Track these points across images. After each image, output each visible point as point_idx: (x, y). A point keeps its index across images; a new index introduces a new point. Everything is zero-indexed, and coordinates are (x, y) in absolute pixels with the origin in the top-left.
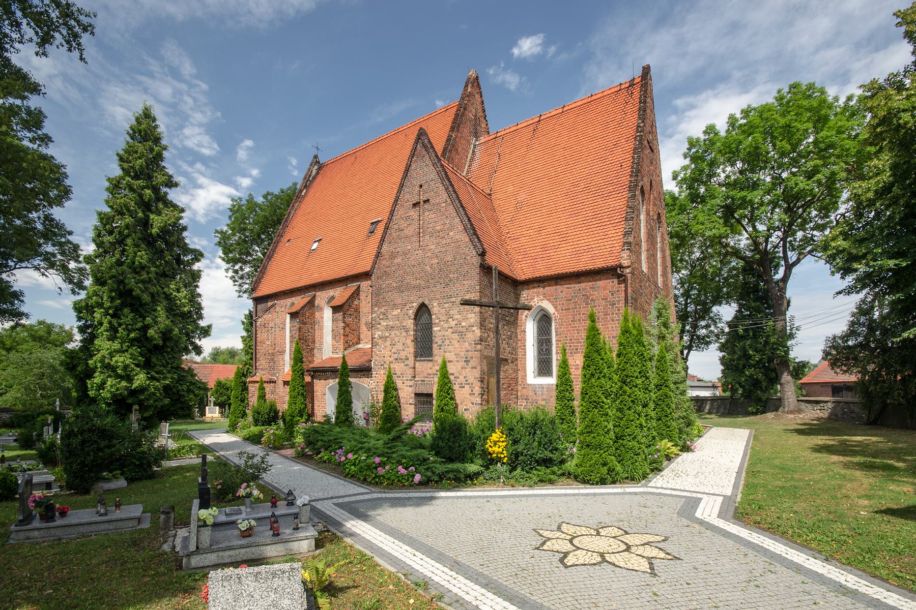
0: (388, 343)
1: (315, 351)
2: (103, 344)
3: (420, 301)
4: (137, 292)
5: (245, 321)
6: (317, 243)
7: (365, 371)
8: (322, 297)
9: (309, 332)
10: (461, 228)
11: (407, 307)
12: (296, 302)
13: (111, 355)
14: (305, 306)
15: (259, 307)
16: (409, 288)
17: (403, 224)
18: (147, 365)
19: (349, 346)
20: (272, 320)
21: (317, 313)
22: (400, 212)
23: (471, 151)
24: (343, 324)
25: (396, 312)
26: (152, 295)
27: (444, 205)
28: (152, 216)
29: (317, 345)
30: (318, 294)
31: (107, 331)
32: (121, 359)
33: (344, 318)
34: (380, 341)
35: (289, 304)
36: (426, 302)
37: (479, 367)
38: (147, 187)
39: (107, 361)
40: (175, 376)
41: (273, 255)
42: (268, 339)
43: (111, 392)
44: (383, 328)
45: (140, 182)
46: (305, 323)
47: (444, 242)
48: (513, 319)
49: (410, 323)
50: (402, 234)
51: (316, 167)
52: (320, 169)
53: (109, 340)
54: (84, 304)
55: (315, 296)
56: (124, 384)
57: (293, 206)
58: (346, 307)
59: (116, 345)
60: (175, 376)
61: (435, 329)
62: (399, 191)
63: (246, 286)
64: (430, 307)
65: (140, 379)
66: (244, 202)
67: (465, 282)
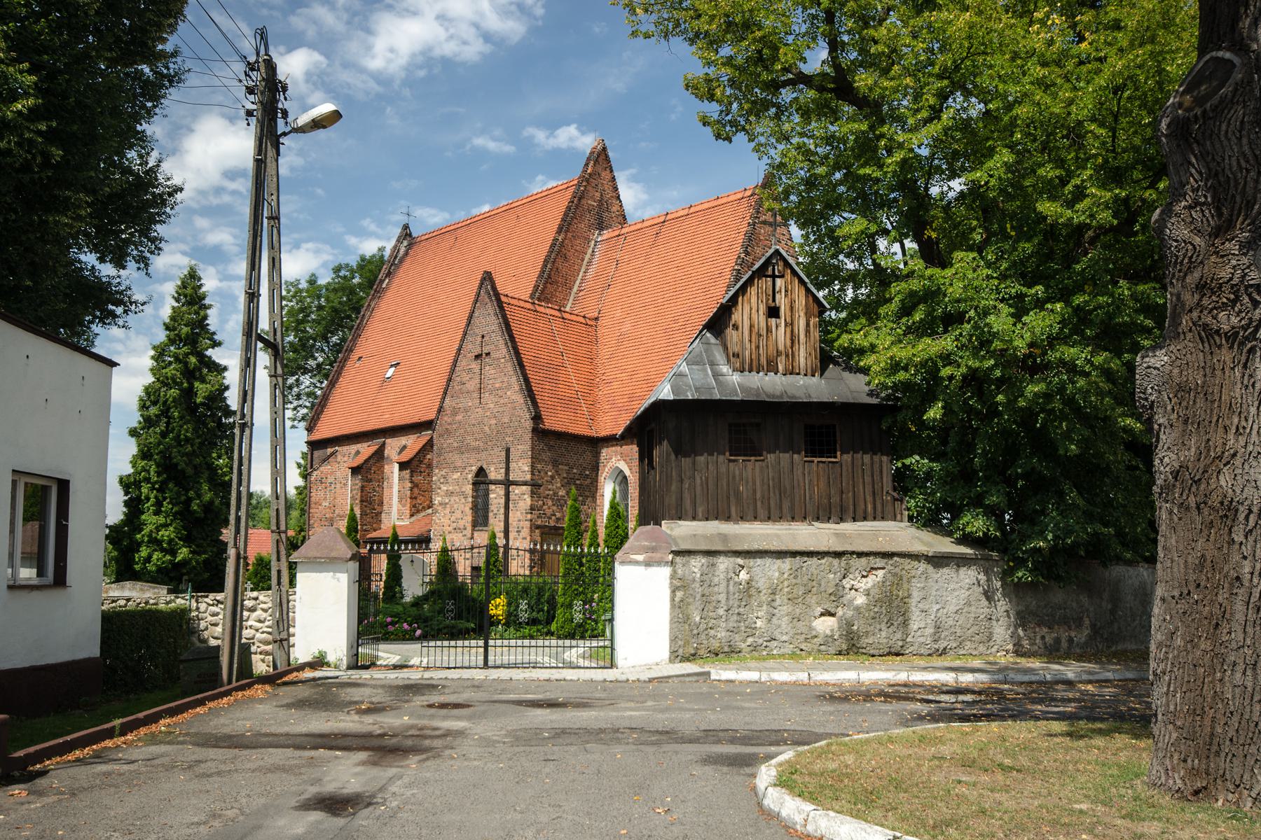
0: (447, 511)
1: (383, 515)
2: (150, 519)
3: (479, 464)
4: (182, 466)
5: (302, 462)
6: (393, 369)
7: (423, 541)
8: (393, 447)
9: (375, 491)
10: (517, 388)
11: (467, 471)
12: (362, 450)
13: (158, 529)
14: (370, 458)
15: (316, 454)
16: (470, 449)
17: (465, 378)
18: (188, 540)
19: (418, 511)
20: (332, 473)
21: (386, 467)
22: (462, 363)
23: (590, 250)
24: (410, 485)
25: (456, 476)
26: (195, 467)
27: (503, 360)
28: (197, 384)
29: (385, 508)
30: (388, 441)
31: (152, 506)
32: (167, 533)
33: (412, 476)
34: (440, 508)
35: (353, 452)
36: (484, 467)
37: (529, 538)
38: (192, 353)
39: (154, 535)
40: (215, 550)
41: (338, 379)
42: (325, 499)
43: (157, 565)
44: (443, 493)
45: (185, 349)
46: (370, 481)
47: (502, 401)
48: (589, 481)
49: (468, 489)
50: (464, 388)
51: (405, 243)
52: (410, 246)
53: (155, 515)
54: (132, 480)
55: (384, 443)
56: (168, 557)
57: (369, 305)
58: (415, 463)
59: (161, 520)
60: (215, 550)
61: (492, 496)
62: (463, 340)
63: (305, 411)
64: (487, 471)
65: (183, 553)
66: (304, 285)
67: (519, 447)
